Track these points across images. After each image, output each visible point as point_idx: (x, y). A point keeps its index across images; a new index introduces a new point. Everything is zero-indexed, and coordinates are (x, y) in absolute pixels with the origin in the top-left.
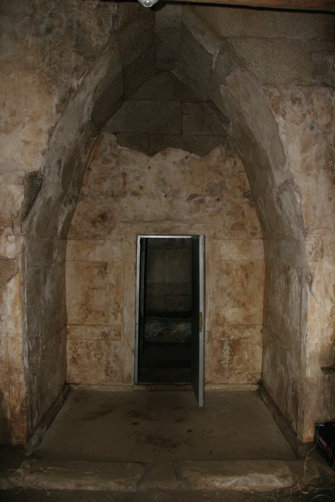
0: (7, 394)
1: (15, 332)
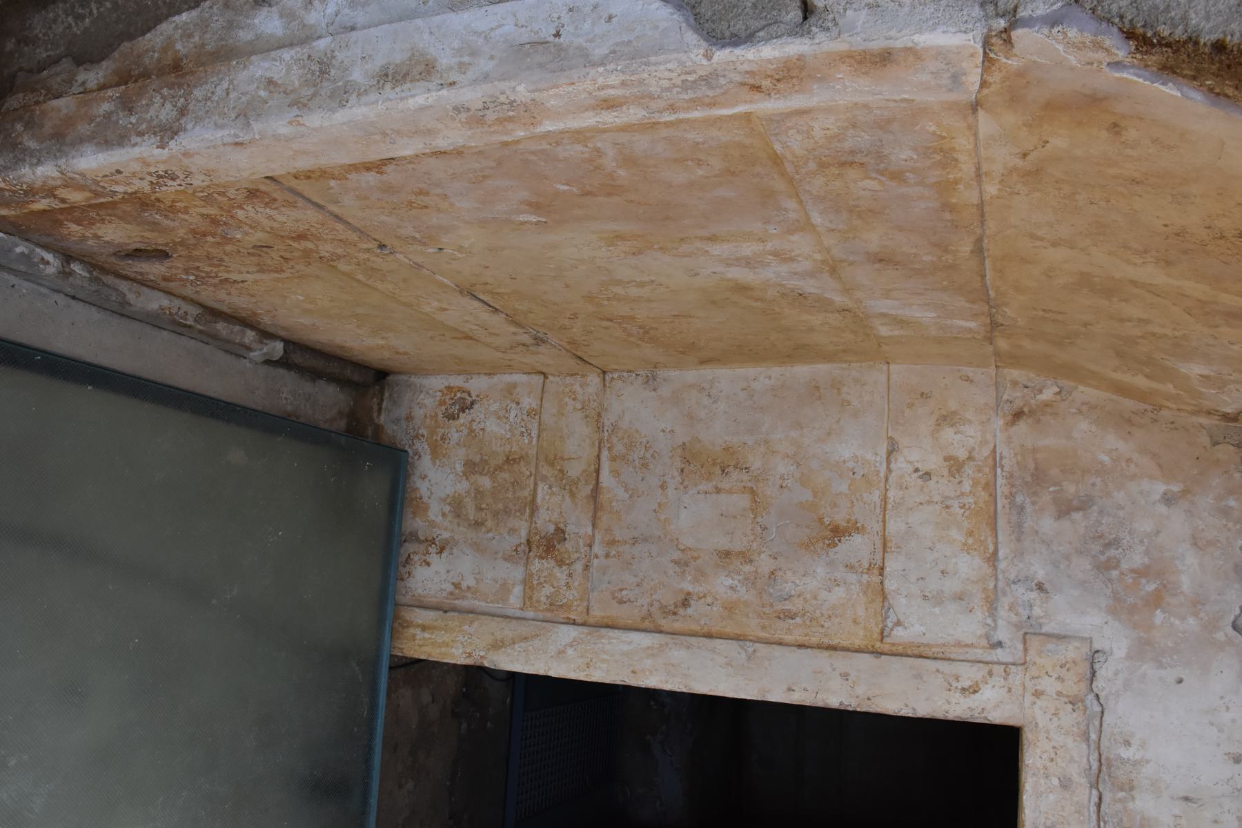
0: (92, 77)
1: (357, 75)
